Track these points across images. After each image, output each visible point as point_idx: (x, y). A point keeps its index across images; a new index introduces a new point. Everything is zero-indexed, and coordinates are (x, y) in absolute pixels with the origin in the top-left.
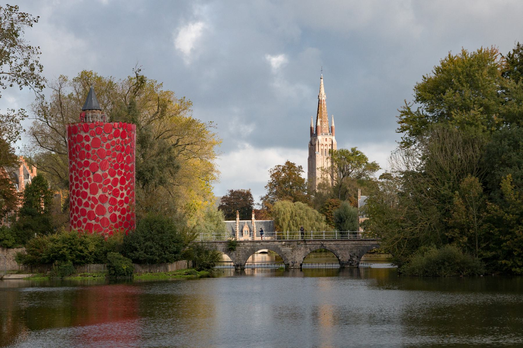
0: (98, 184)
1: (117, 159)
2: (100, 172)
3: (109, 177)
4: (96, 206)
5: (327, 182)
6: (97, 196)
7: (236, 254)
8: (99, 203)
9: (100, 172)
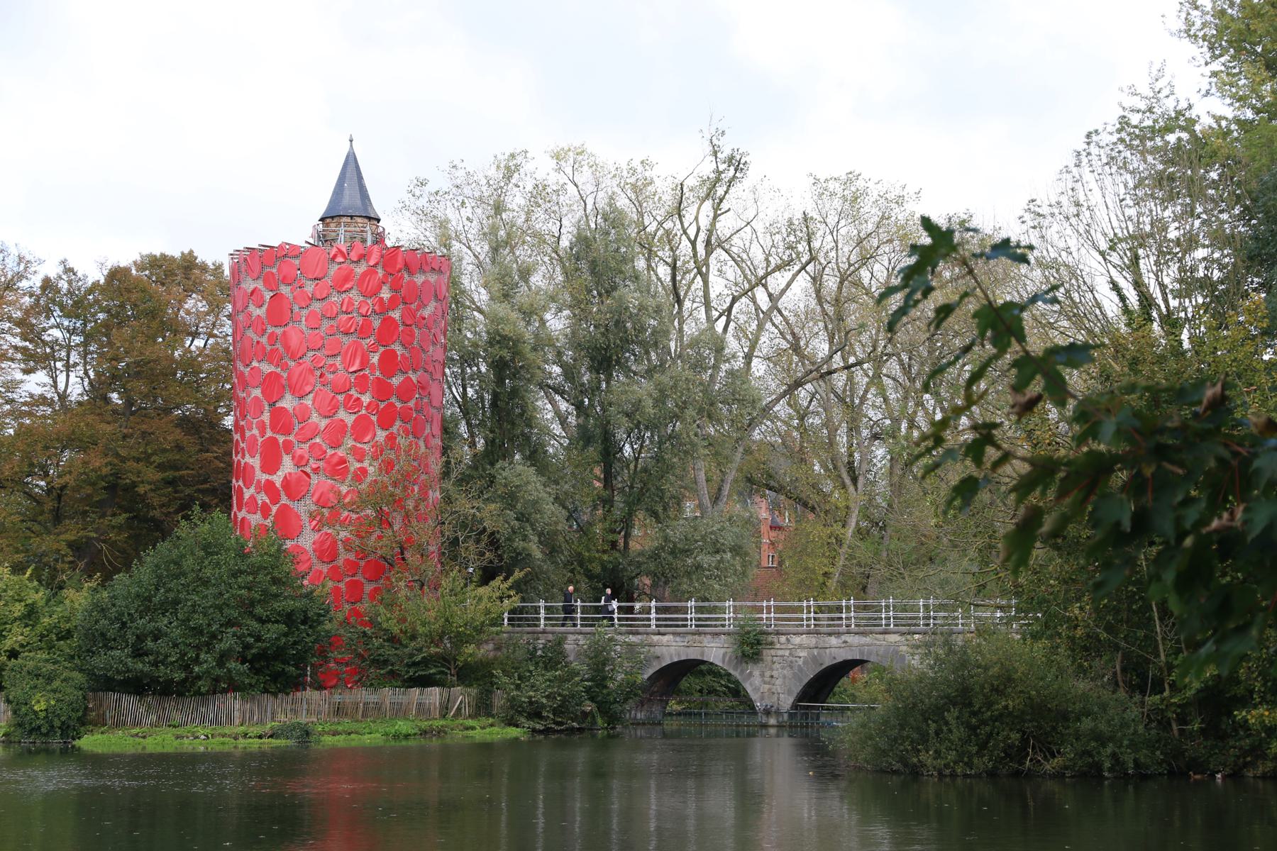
0: (281, 439)
1: (343, 362)
2: (288, 402)
3: (315, 418)
4: (274, 509)
5: (953, 499)
6: (278, 479)
7: (762, 675)
8: (284, 500)
9: (288, 402)
